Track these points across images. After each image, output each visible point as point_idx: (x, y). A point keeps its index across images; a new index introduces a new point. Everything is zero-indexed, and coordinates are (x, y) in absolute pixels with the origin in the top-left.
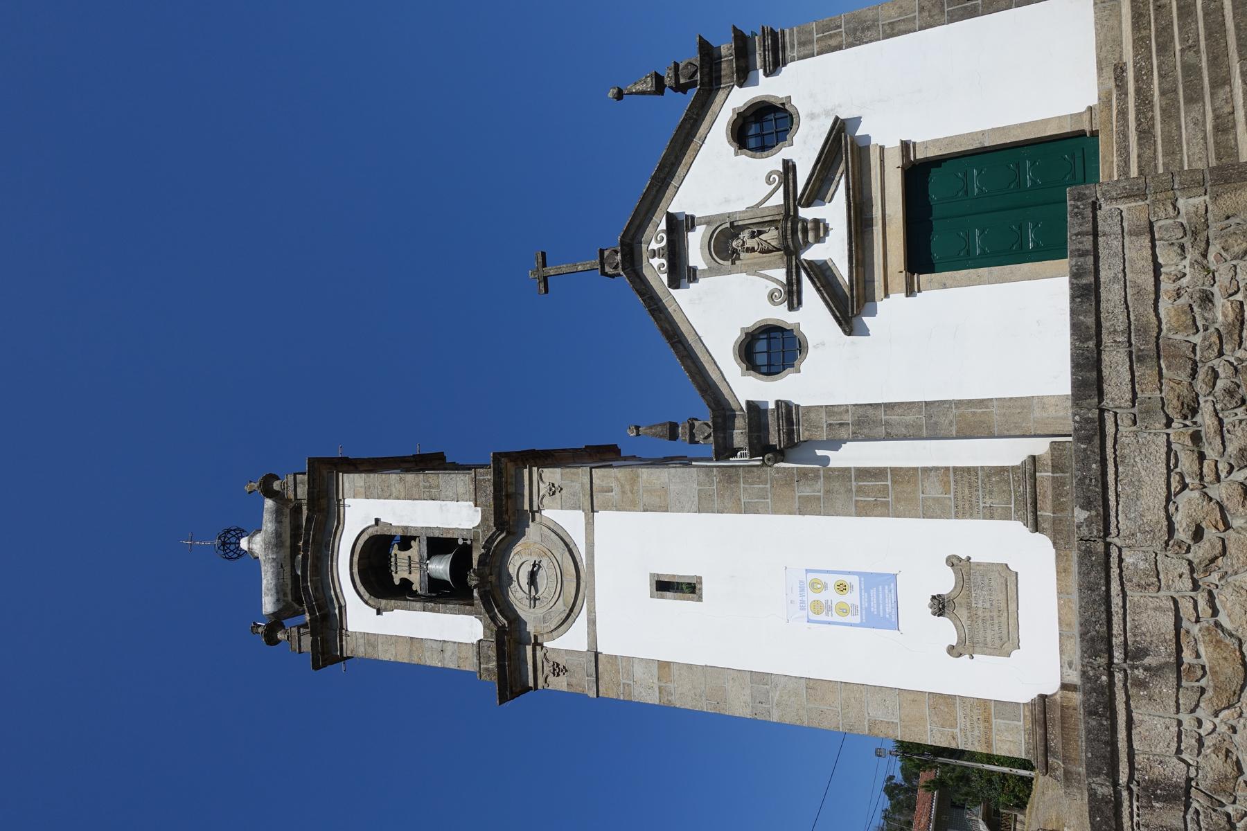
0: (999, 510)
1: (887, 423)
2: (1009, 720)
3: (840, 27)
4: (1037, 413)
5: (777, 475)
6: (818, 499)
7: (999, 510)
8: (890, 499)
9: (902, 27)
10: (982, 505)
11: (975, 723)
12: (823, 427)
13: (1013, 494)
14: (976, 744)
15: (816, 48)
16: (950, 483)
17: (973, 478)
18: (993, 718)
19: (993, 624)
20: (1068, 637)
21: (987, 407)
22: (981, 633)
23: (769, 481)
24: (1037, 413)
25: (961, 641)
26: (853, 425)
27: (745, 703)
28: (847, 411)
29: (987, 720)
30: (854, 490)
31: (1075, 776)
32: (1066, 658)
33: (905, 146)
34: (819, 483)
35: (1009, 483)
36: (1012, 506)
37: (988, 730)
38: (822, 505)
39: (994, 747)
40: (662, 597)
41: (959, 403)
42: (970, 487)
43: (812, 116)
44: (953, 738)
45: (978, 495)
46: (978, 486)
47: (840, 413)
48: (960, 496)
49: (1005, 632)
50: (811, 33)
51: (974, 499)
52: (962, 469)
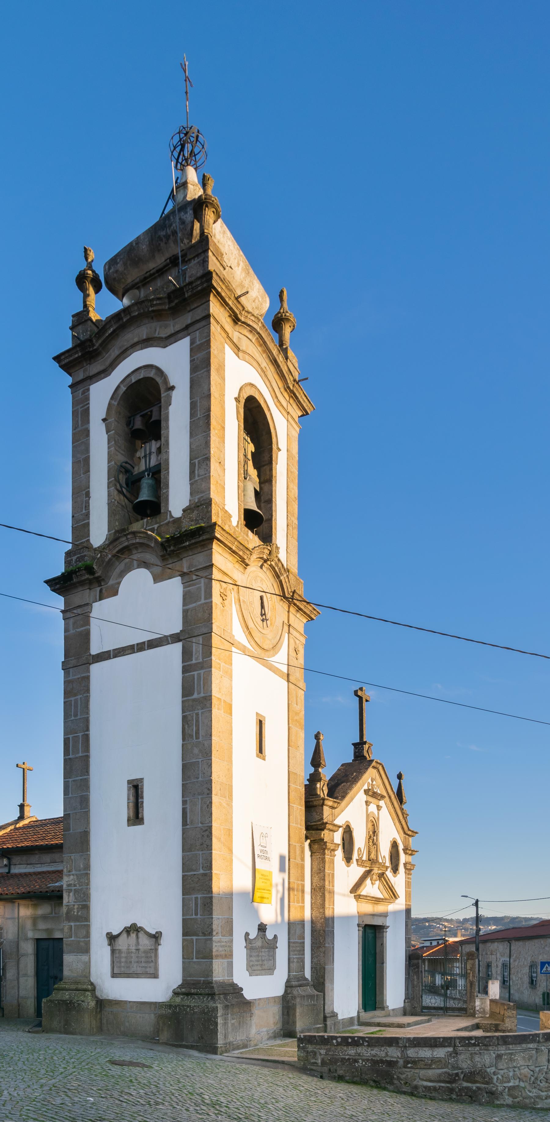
36: (294, 974)
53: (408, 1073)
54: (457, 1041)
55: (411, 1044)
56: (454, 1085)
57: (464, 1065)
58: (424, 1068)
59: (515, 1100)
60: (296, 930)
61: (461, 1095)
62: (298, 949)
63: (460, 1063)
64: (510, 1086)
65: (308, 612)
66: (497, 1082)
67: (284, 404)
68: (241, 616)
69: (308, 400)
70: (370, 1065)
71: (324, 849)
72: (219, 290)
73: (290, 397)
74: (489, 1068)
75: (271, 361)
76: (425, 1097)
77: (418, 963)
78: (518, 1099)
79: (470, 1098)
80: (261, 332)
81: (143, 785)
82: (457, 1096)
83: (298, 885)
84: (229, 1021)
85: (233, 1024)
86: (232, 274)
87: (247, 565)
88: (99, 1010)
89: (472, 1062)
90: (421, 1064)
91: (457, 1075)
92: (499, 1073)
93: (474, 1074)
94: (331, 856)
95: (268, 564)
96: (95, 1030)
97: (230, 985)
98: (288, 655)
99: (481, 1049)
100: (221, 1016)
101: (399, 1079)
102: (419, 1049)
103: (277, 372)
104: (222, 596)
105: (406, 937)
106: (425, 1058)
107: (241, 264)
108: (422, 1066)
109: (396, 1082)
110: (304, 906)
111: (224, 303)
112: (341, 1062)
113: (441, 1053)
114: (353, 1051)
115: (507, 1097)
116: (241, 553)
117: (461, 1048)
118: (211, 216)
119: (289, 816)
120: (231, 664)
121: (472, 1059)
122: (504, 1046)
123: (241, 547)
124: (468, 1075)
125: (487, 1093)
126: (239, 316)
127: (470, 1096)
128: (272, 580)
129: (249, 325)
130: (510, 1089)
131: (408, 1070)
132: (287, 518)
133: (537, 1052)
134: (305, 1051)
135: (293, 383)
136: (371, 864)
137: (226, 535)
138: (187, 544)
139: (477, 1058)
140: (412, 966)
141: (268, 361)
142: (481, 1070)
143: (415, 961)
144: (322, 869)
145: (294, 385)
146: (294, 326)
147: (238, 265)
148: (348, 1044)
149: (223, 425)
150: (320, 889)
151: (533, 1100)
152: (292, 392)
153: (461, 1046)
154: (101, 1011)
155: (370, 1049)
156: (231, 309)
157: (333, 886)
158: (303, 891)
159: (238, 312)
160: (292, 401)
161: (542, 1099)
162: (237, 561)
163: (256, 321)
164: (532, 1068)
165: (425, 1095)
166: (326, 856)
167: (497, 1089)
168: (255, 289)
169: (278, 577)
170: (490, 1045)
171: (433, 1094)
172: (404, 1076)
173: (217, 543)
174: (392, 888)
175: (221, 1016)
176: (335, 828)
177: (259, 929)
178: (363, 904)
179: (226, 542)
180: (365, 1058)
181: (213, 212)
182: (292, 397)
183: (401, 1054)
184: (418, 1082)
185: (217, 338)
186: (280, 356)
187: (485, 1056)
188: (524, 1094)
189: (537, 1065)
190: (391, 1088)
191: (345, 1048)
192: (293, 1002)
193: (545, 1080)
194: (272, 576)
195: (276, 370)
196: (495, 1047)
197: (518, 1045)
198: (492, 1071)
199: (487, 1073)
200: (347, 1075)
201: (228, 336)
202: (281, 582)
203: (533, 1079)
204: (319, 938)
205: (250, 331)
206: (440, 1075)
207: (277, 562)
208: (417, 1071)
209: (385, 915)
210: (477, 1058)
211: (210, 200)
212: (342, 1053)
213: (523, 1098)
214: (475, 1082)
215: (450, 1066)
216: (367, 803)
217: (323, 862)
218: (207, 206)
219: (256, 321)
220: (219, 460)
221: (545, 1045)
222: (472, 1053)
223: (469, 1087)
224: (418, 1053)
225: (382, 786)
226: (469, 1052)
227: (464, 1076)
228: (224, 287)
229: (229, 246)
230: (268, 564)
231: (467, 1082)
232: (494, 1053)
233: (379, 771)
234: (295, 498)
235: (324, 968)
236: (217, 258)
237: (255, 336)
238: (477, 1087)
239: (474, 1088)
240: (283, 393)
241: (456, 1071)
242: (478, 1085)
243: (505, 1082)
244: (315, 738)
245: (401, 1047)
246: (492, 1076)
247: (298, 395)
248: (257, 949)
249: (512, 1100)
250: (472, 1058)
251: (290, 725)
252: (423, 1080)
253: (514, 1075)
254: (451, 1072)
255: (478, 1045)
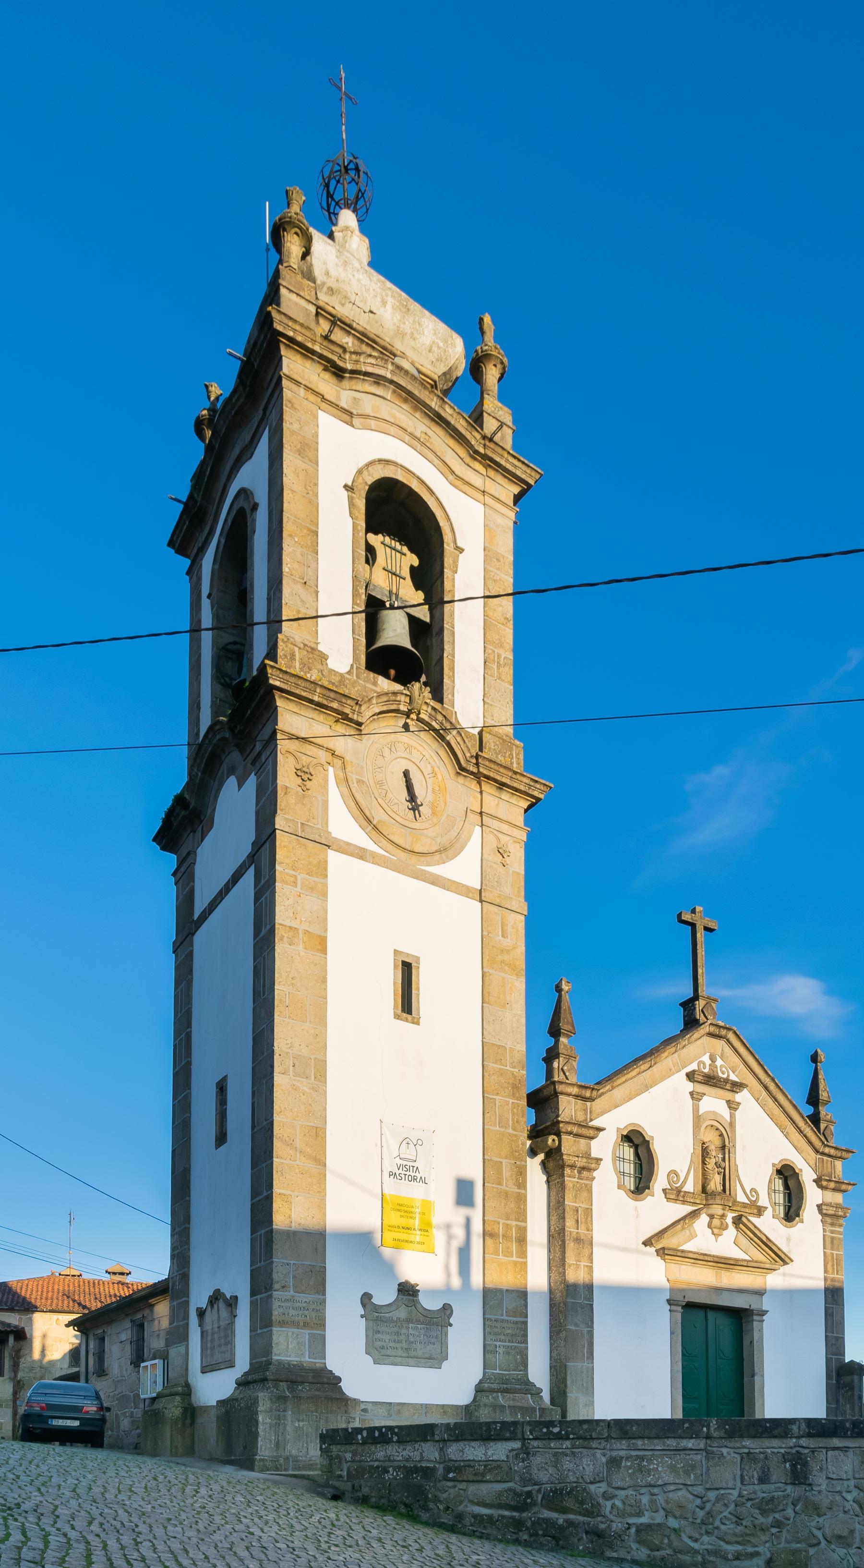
0: (494, 1359)
1: (578, 1266)
2: (309, 1347)
3: (837, 1274)
4: (582, 1399)
5: (520, 1143)
6: (500, 1183)
7: (494, 1359)
8: (501, 1257)
9: (830, 1323)
10: (498, 1344)
11: (301, 1312)
12: (575, 1202)
13: (507, 1373)
14: (281, 1310)
15: (828, 1251)
16: (515, 1317)
17: (519, 1339)
18: (309, 1332)
19: (395, 1341)
20: (389, 1411)
21: (588, 1358)
22: (386, 1329)
23: (515, 1133)
24: (582, 1399)
25: (377, 1308)
26: (577, 1233)
27: (291, 1043)
28: (588, 1230)
29: (306, 1325)
30: (509, 1222)
31: (282, 1406)
32: (369, 1407)
33: (763, 1313)
34: (514, 1187)
35: (515, 1370)
36: (498, 1371)
37: (296, 1325)
38: (494, 1186)
39: (281, 1329)
40: (395, 966)
41: (591, 1334)
42: (512, 1335)
43: (788, 1239)
44: (283, 1287)
45: (505, 1342)
46: (513, 1342)
47: (586, 1223)
48: (505, 1325)
49: (389, 1352)
50: (838, 1250)
51: (502, 1337)
52: (526, 1330)
53: (452, 1490)
54: (527, 1429)
55: (451, 1435)
56: (524, 1515)
57: (543, 1477)
58: (473, 1481)
59: (656, 1553)
60: (502, 1300)
61: (537, 1535)
62: (509, 1331)
63: (534, 1471)
64: (641, 1524)
65: (522, 788)
66: (611, 1513)
67: (477, 481)
68: (352, 804)
69: (523, 463)
70: (402, 1476)
71: (562, 1167)
72: (291, 334)
73: (487, 467)
74: (591, 1483)
75: (433, 420)
76: (472, 1534)
77: (853, 1381)
78: (662, 1553)
79: (554, 1542)
80: (395, 379)
81: (226, 1085)
82: (531, 1535)
83: (508, 1227)
84: (289, 1424)
85: (297, 1429)
86: (377, 322)
87: (360, 724)
88: (188, 1422)
89: (559, 1470)
90: (468, 1474)
91: (529, 1494)
92: (615, 1496)
93: (561, 1493)
94: (579, 1178)
95: (412, 720)
96: (180, 1450)
97: (310, 1370)
98: (482, 860)
99: (574, 1446)
100: (266, 1411)
101: (436, 1500)
102: (465, 1445)
103: (450, 435)
104: (299, 773)
105: (826, 1337)
106: (474, 1460)
107: (390, 301)
108: (471, 1478)
109: (431, 1505)
110: (526, 1263)
111: (307, 352)
112: (369, 1472)
113: (499, 1451)
114: (382, 1453)
115: (634, 1546)
116: (335, 705)
117: (535, 1443)
118: (293, 241)
119: (483, 1114)
120: (326, 876)
121: (556, 1464)
122: (624, 1442)
123: (332, 695)
124: (549, 1496)
125: (587, 1533)
126: (341, 364)
127: (554, 1537)
128: (435, 745)
129: (366, 374)
130: (641, 1529)
131: (450, 1484)
132: (485, 651)
133: (707, 1459)
134: (328, 1456)
135: (483, 442)
136: (706, 1200)
137: (293, 680)
138: (249, 712)
139: (567, 1464)
140: (842, 1388)
141: (427, 422)
142: (576, 1487)
143: (847, 1379)
144: (561, 1200)
145: (485, 445)
146: (502, 363)
147: (384, 303)
148: (376, 1441)
149: (314, 529)
150: (559, 1234)
151: (700, 1558)
152: (485, 457)
153: (535, 1439)
154: (193, 1423)
155: (401, 1447)
156: (321, 356)
157: (589, 1229)
158: (522, 1240)
159: (335, 358)
160: (491, 473)
161: (727, 1559)
162: (336, 721)
163: (380, 363)
164: (699, 1490)
165: (474, 1531)
166: (566, 1178)
167: (609, 1527)
168: (426, 332)
169: (443, 738)
170: (592, 1439)
171: (489, 1531)
172: (445, 1495)
173: (282, 697)
174: (768, 1243)
175: (266, 1411)
176: (591, 1133)
177: (399, 1290)
178: (683, 1267)
179: (297, 691)
180: (396, 1464)
181: (296, 233)
182: (490, 466)
183: (440, 1454)
184: (466, 1506)
185: (296, 406)
186: (447, 408)
187: (584, 1460)
188: (676, 1544)
189: (708, 1486)
190: (425, 1516)
191: (373, 1448)
192: (476, 1414)
193: (735, 1519)
194: (433, 739)
195: (447, 431)
196: (603, 1444)
197: (656, 1441)
198: (602, 1490)
199: (588, 1493)
200: (373, 1494)
201: (323, 398)
202: (449, 744)
203: (701, 1514)
204: (559, 1317)
205: (375, 382)
206: (500, 1494)
207: (433, 713)
208: (463, 1486)
209: (760, 1293)
210: (567, 1464)
211: (285, 218)
212: (369, 1457)
213: (674, 1551)
214: (565, 1510)
215: (517, 1478)
216: (695, 1097)
217: (562, 1189)
218: (284, 230)
219: (380, 363)
220: (303, 579)
221: (729, 1444)
222: (556, 1453)
223: (551, 1519)
224: (462, 1451)
225: (742, 1066)
226: (551, 1451)
227: (543, 1498)
228: (298, 328)
229: (359, 280)
230: (412, 720)
231: (550, 1509)
232: (604, 1455)
233: (729, 1042)
234: (506, 619)
235: (565, 1366)
236: (298, 295)
237: (389, 388)
238: (566, 1521)
239: (561, 1522)
240: (471, 464)
241: (529, 1488)
242: (571, 1516)
243: (631, 1515)
244: (556, 991)
245: (437, 1441)
246: (601, 1501)
247: (498, 459)
248: (393, 1322)
249: (648, 1552)
250: (557, 1462)
251: (485, 970)
252: (472, 1502)
253: (652, 1502)
254: (518, 1488)
255: (568, 1438)
